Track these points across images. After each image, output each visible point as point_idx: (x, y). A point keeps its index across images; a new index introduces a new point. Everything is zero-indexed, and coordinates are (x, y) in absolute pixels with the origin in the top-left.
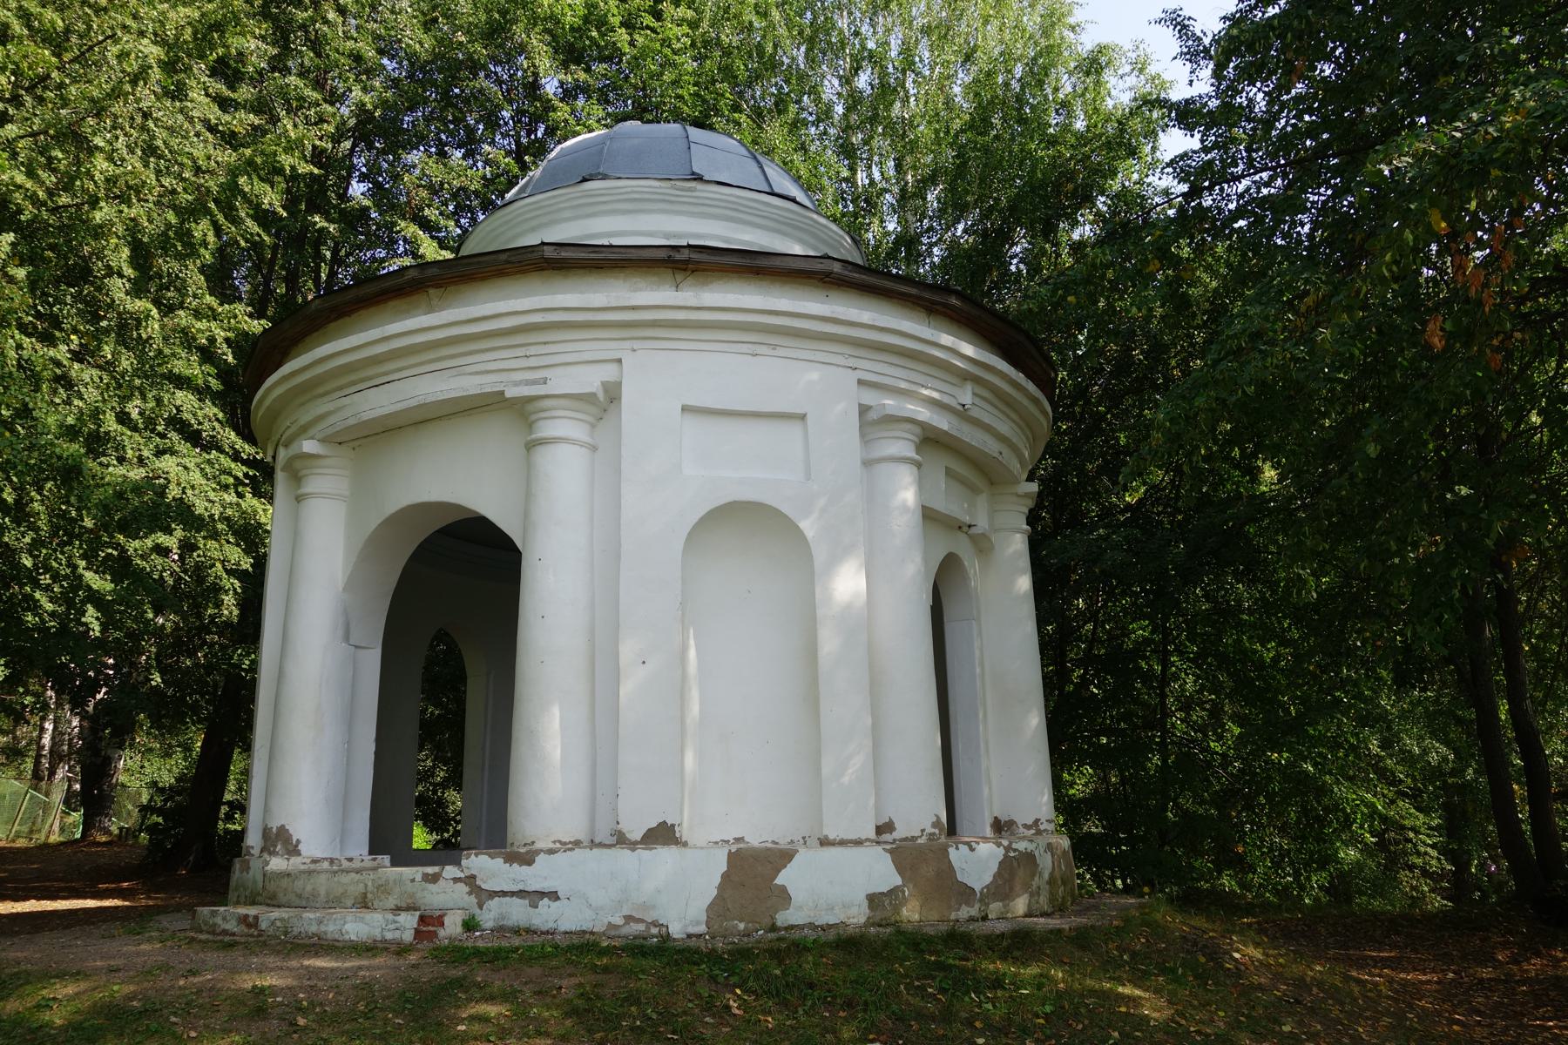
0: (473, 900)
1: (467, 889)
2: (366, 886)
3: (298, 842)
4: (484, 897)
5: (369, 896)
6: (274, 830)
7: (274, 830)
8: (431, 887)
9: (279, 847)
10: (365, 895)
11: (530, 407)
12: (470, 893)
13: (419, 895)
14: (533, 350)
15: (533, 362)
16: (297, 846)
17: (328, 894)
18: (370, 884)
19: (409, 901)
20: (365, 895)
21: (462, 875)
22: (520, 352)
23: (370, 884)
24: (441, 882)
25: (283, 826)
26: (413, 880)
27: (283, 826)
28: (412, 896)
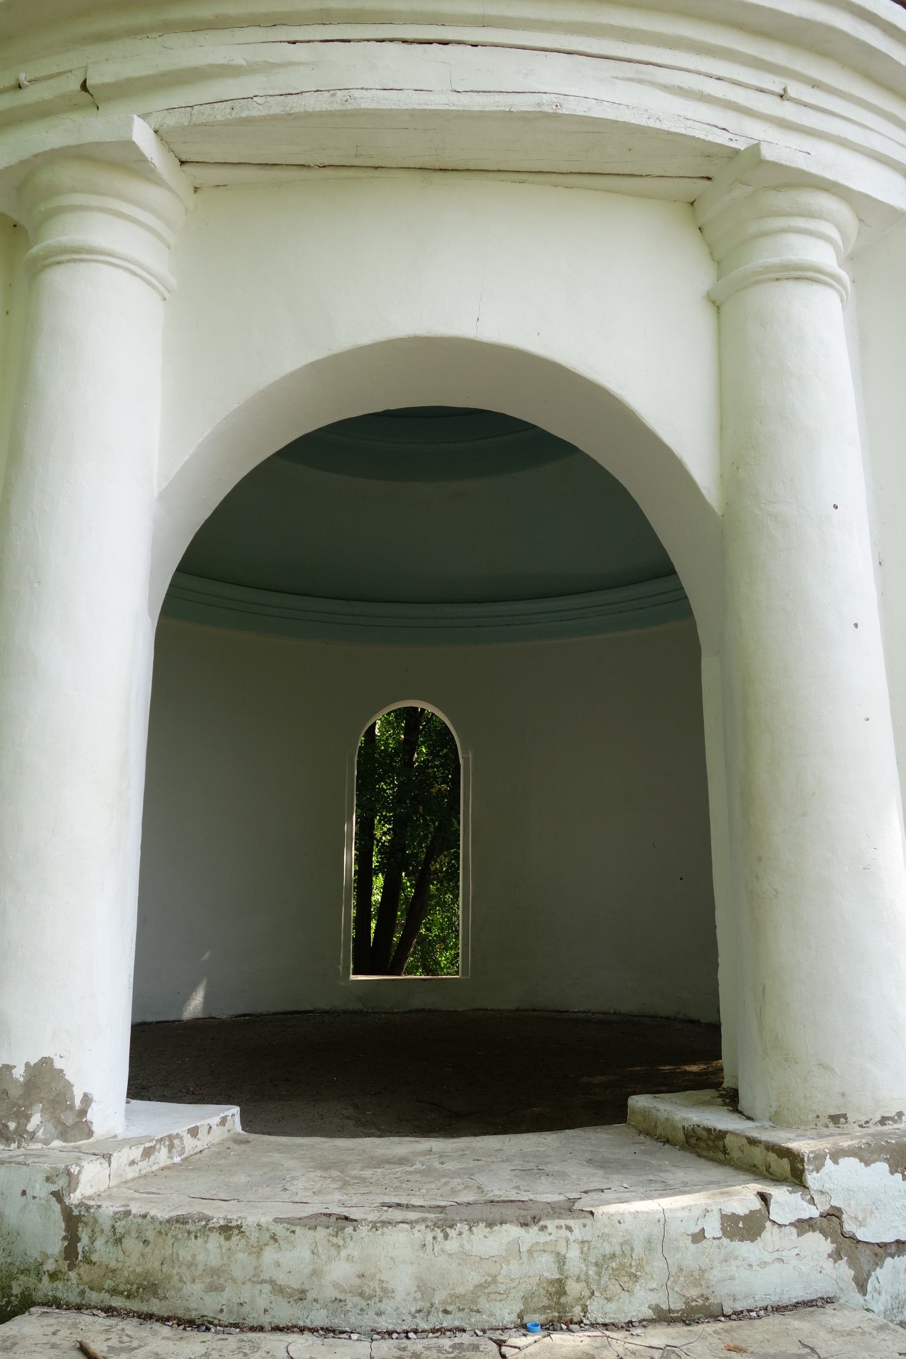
0: (844, 1271)
1: (827, 1246)
2: (561, 1260)
3: (87, 1100)
4: (865, 1257)
5: (574, 1288)
6: (19, 1073)
7: (19, 1073)
8: (744, 1248)
9: (36, 1119)
10: (559, 1288)
11: (781, 200)
12: (836, 1256)
13: (715, 1275)
14: (796, 89)
15: (786, 111)
16: (83, 1112)
17: (423, 1289)
18: (573, 1254)
19: (693, 1293)
20: (559, 1288)
21: (813, 1212)
22: (774, 83)
23: (573, 1254)
24: (770, 1234)
25: (46, 1062)
26: (699, 1237)
27: (892, 1173)
28: (698, 1277)
